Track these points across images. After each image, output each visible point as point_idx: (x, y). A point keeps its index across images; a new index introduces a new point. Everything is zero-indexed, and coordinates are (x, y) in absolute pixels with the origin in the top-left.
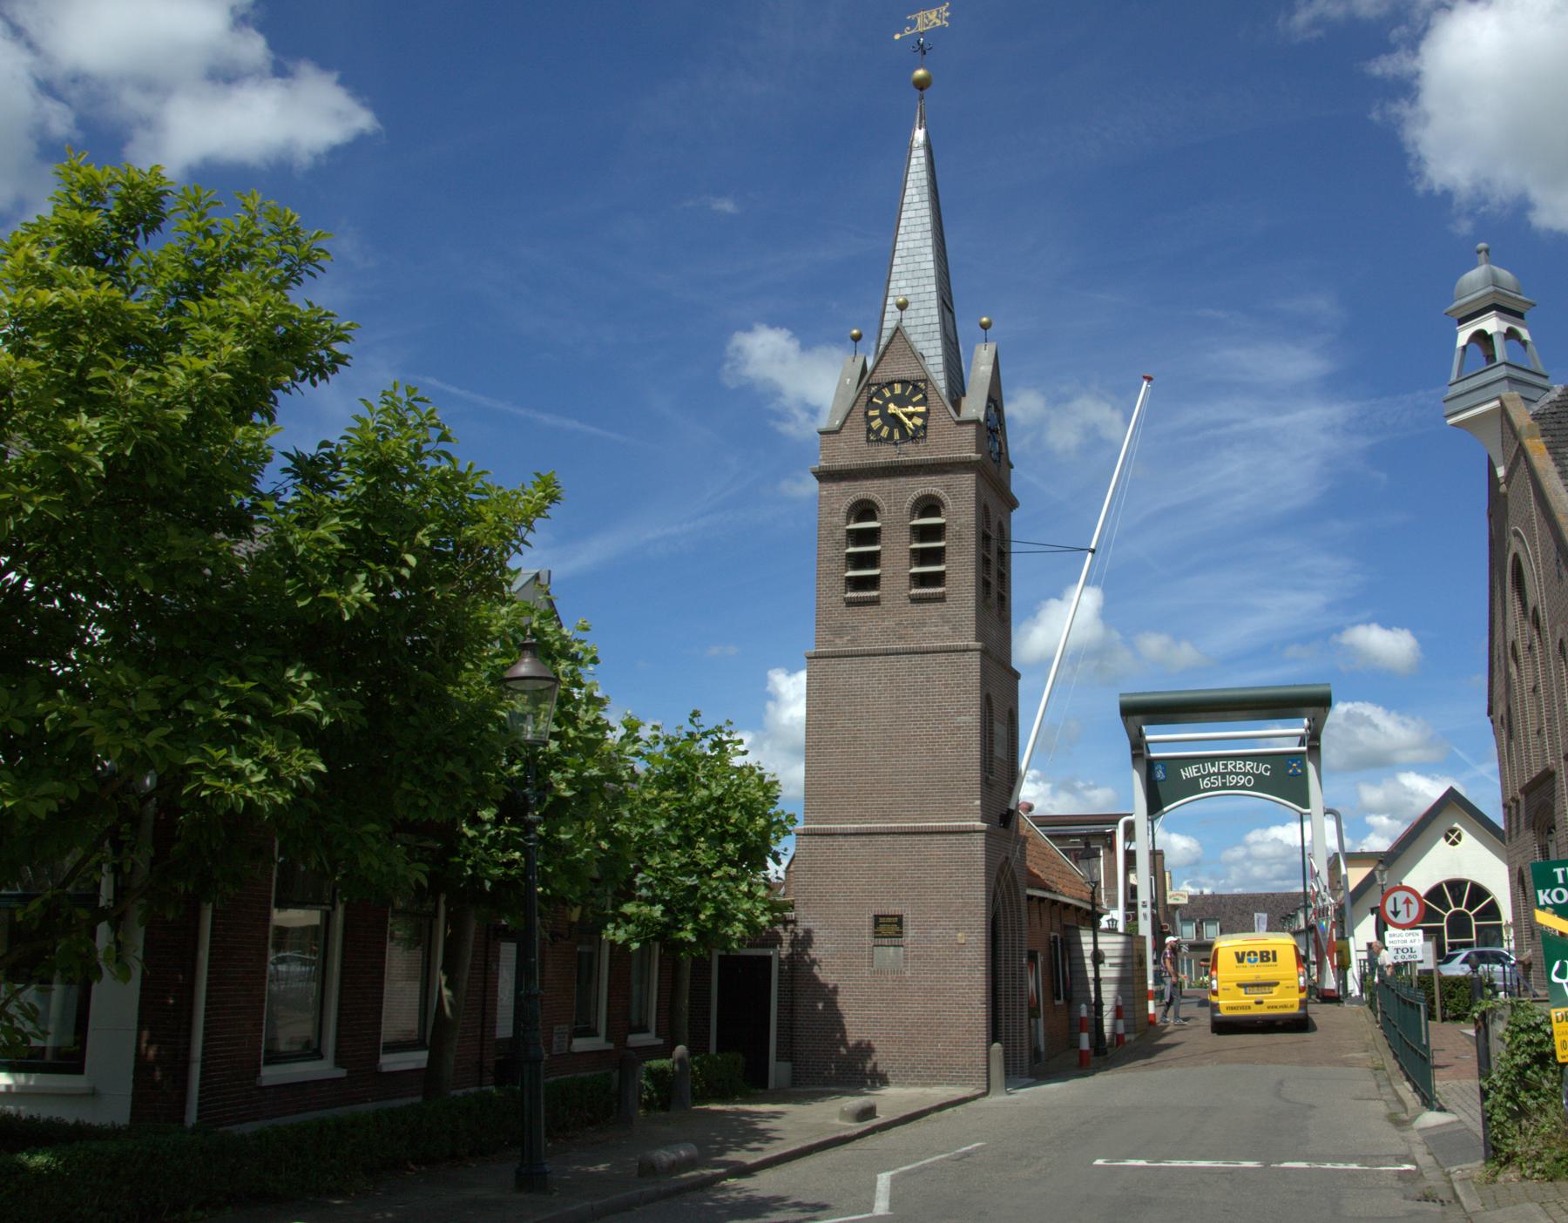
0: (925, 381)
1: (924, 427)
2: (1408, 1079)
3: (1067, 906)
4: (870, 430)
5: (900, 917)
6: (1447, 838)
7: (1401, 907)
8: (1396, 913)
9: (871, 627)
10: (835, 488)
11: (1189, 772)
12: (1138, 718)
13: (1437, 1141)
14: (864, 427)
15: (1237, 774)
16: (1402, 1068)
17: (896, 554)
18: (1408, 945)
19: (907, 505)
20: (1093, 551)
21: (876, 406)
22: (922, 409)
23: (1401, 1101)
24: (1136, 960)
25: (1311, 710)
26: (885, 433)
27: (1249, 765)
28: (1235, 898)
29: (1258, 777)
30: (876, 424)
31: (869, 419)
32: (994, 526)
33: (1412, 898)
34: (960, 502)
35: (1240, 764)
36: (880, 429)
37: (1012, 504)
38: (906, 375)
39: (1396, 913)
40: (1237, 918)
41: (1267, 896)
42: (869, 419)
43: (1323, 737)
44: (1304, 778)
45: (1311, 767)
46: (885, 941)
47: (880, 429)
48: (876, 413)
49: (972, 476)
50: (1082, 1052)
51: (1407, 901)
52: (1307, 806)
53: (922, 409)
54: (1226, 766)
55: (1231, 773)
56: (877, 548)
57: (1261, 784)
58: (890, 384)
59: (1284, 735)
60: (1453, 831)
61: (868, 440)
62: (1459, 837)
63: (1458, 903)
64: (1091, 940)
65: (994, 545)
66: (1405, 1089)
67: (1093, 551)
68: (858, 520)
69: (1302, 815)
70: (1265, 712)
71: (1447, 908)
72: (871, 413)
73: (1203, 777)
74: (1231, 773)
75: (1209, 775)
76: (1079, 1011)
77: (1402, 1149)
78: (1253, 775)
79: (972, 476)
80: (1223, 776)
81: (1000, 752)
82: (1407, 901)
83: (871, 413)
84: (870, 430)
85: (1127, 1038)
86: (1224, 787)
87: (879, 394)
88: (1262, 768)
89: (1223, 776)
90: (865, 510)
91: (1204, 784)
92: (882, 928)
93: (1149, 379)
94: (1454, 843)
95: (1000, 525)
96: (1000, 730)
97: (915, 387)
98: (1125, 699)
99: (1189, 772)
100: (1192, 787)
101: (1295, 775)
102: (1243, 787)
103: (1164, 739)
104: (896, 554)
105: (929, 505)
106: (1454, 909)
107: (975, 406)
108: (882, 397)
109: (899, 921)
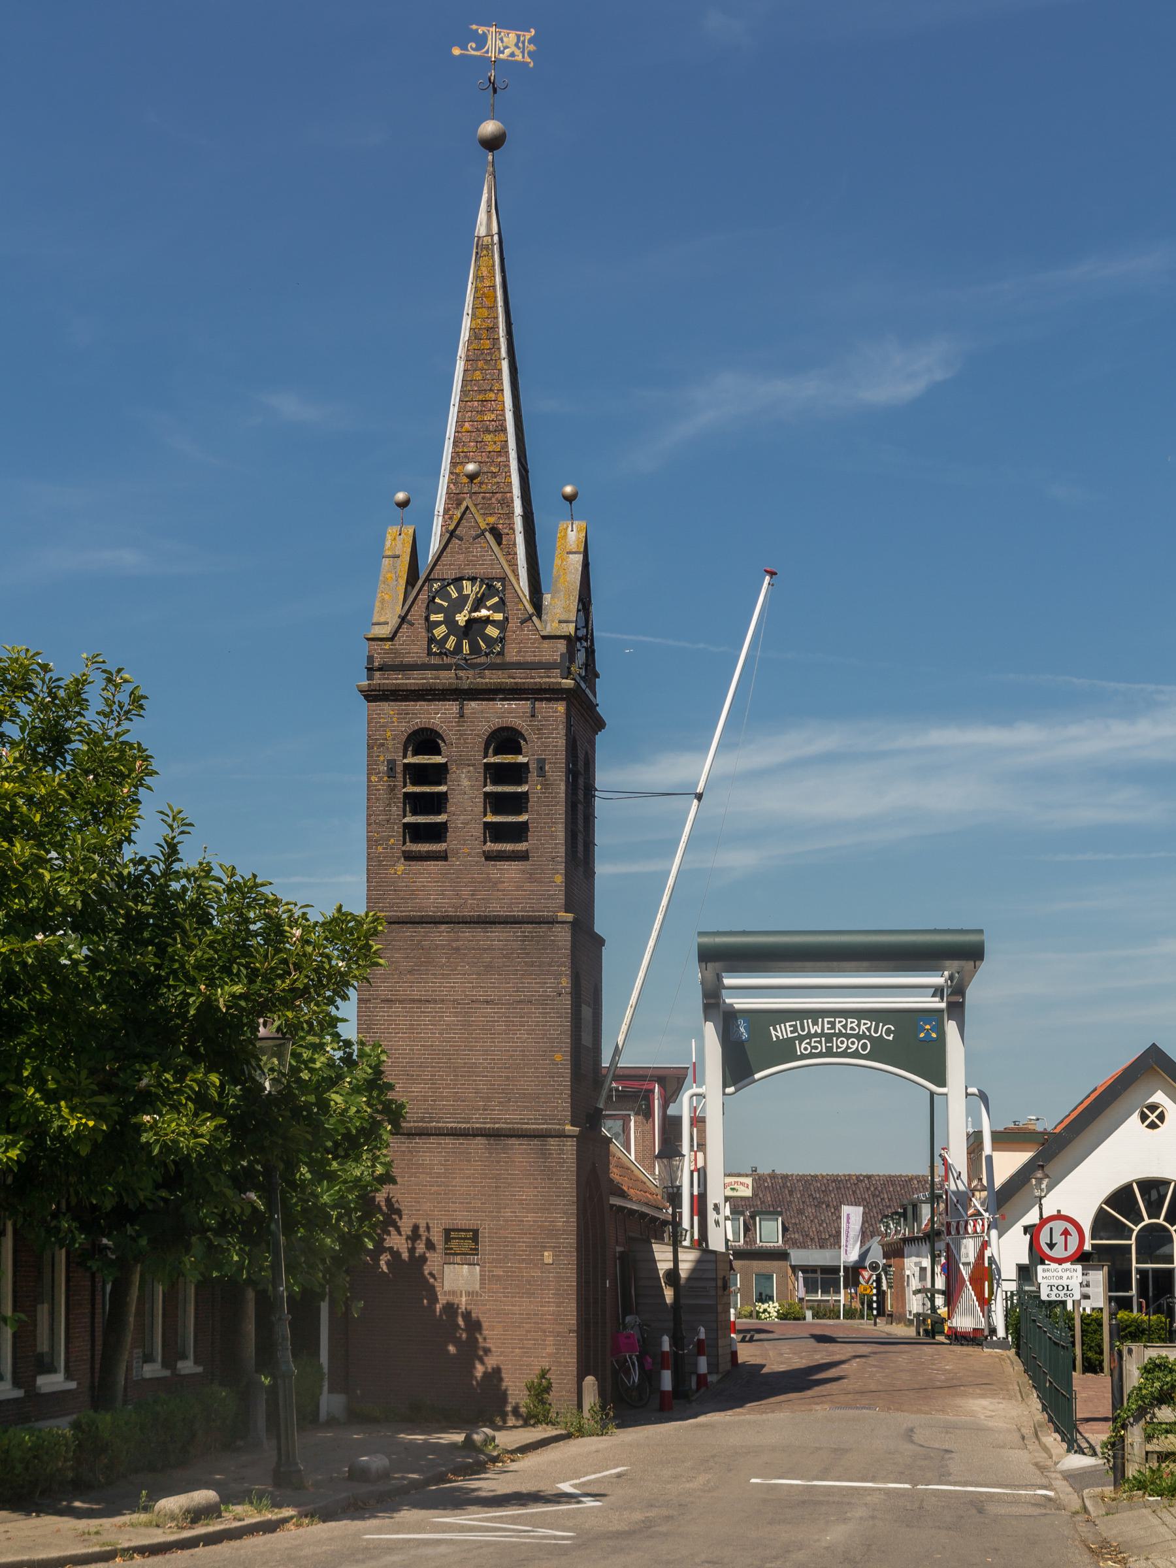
0: (503, 579)
1: (502, 640)
2: (1057, 1430)
3: (632, 1212)
4: (432, 640)
5: (476, 1232)
6: (1144, 1117)
7: (1058, 1239)
8: (1051, 1246)
9: (428, 886)
10: (388, 709)
11: (782, 1032)
12: (718, 965)
13: (1076, 1479)
14: (424, 634)
15: (848, 1036)
16: (1051, 1420)
17: (466, 792)
18: (1064, 1282)
19: (480, 742)
20: (699, 797)
21: (440, 609)
22: (499, 617)
23: (1046, 1449)
24: (720, 1283)
25: (955, 965)
26: (451, 643)
27: (865, 1025)
28: (808, 1182)
29: (877, 1042)
30: (440, 631)
31: (431, 626)
32: (581, 764)
33: (1071, 1228)
34: (545, 731)
35: (852, 1023)
36: (445, 638)
37: (599, 724)
38: (480, 571)
39: (1051, 1246)
40: (810, 1211)
41: (859, 1179)
42: (431, 626)
43: (969, 992)
44: (939, 1047)
45: (951, 1027)
46: (458, 1259)
47: (445, 638)
48: (439, 617)
49: (561, 707)
50: (663, 1393)
51: (1066, 1233)
52: (942, 1083)
53: (499, 617)
54: (833, 1024)
55: (840, 1035)
56: (443, 788)
57: (879, 1051)
58: (457, 581)
59: (915, 992)
60: (1153, 1108)
61: (429, 649)
62: (1161, 1117)
63: (1154, 1212)
64: (670, 1256)
65: (581, 781)
66: (1052, 1439)
67: (699, 797)
68: (416, 753)
69: (932, 1094)
70: (865, 964)
71: (1127, 1233)
72: (433, 618)
73: (801, 1039)
74: (840, 1035)
75: (809, 1036)
76: (660, 1344)
77: (1045, 1481)
78: (870, 1038)
79: (561, 707)
80: (829, 1038)
81: (586, 1040)
82: (1066, 1233)
83: (433, 618)
84: (432, 640)
85: (710, 1378)
86: (829, 1053)
87: (443, 592)
88: (883, 1029)
89: (829, 1038)
90: (425, 741)
91: (802, 1048)
92: (454, 1244)
93: (772, 574)
94: (1153, 1126)
95: (587, 753)
96: (586, 1012)
97: (489, 586)
98: (705, 940)
99: (782, 1032)
100: (786, 1051)
101: (928, 1041)
102: (855, 1054)
103: (748, 991)
104: (466, 792)
105: (506, 740)
106: (1147, 1221)
107: (560, 609)
108: (447, 597)
109: (475, 1235)
